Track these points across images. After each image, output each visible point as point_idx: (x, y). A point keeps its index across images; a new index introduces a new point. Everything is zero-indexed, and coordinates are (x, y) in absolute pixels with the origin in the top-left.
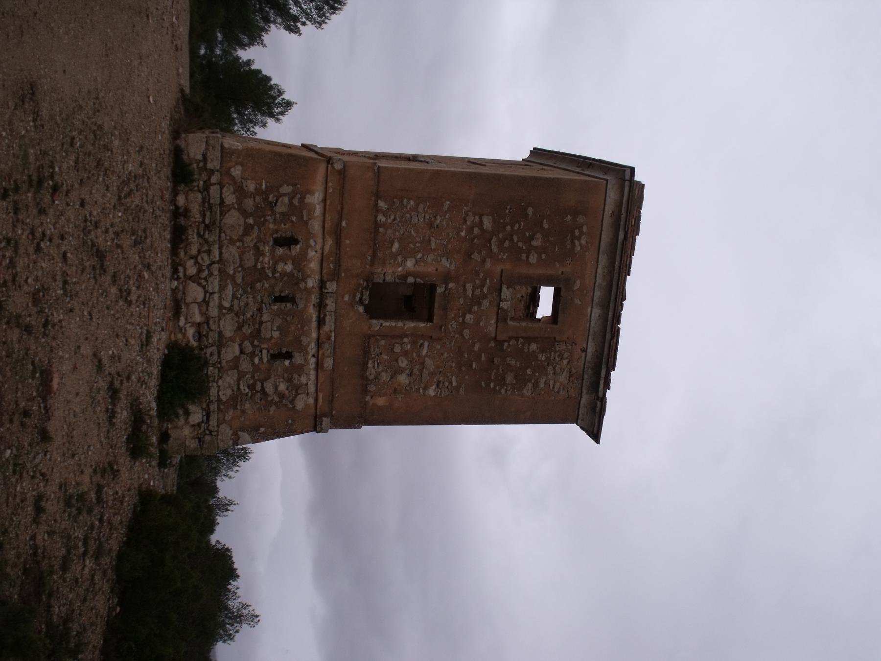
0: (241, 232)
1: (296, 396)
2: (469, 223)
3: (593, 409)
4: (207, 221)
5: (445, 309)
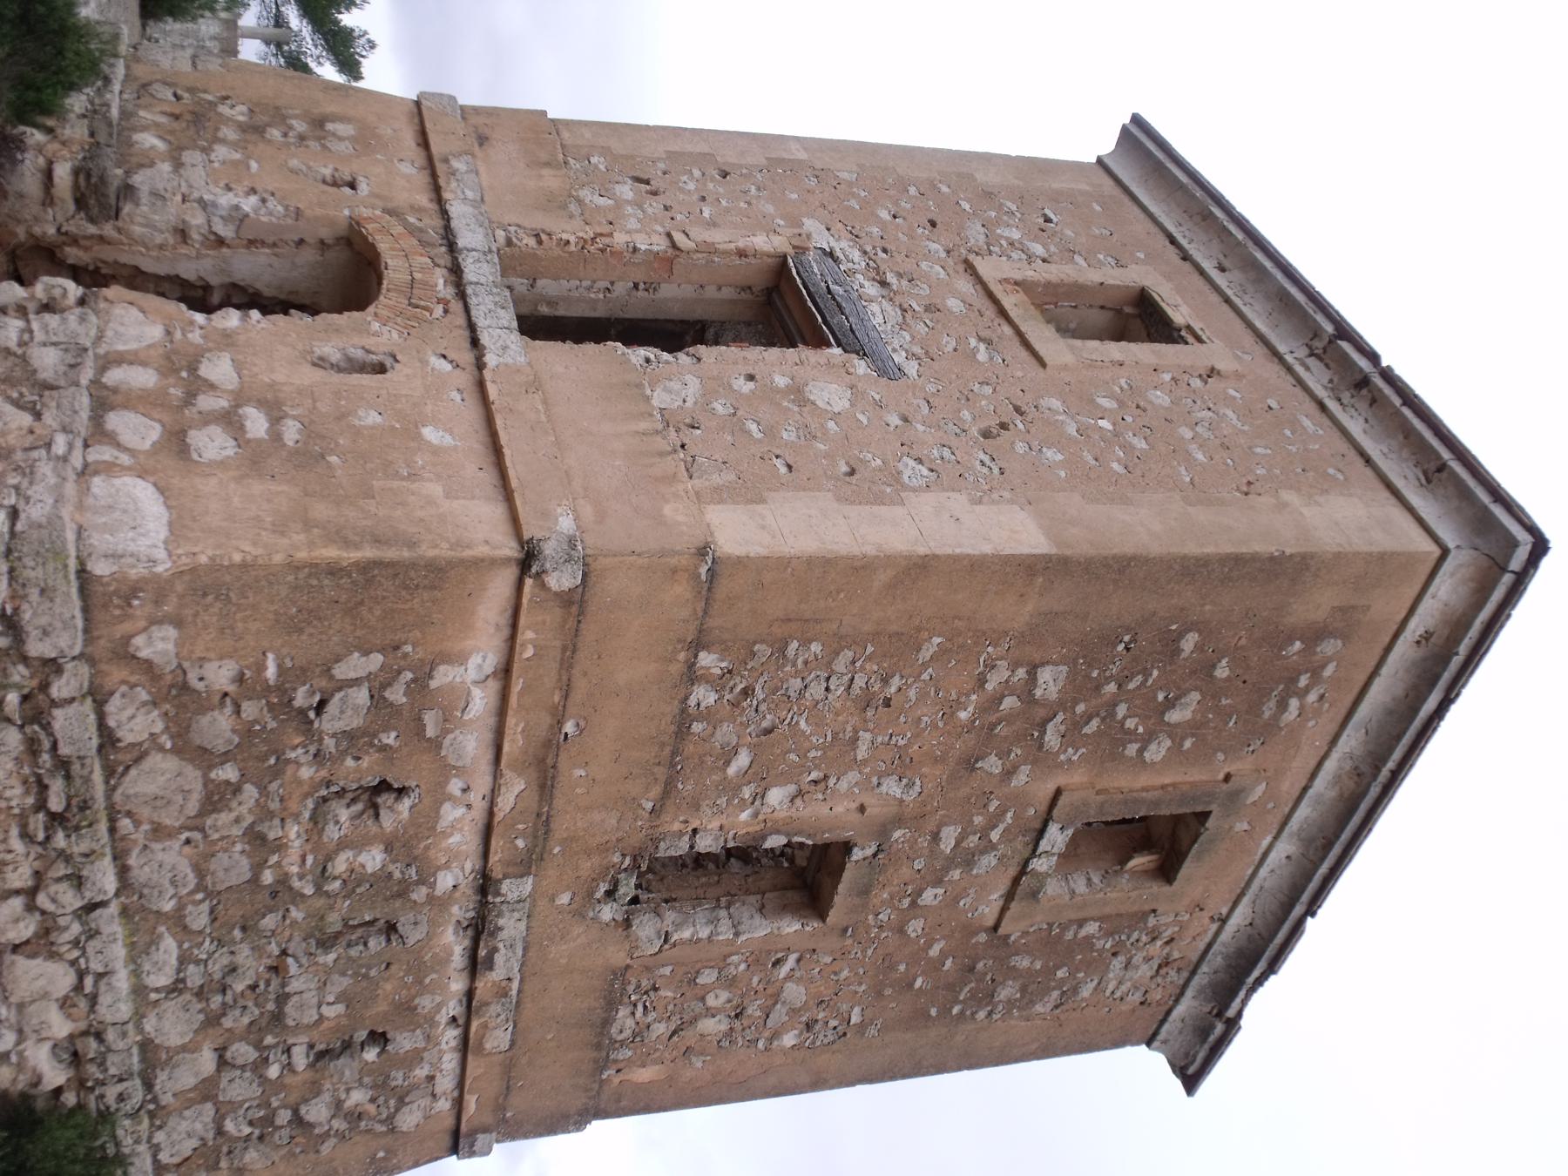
0: (193, 807)
1: (397, 1110)
2: (989, 687)
3: (1203, 1032)
4: (56, 803)
5: (865, 891)
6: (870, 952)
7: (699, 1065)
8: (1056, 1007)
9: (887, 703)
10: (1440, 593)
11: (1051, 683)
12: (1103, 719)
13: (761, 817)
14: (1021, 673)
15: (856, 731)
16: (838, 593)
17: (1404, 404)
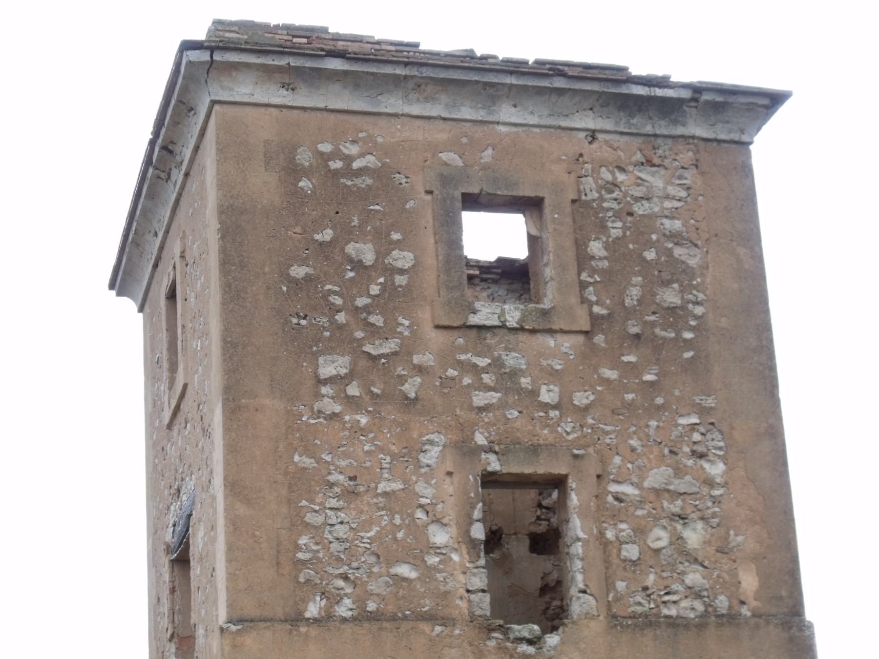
2: (338, 409)
3: (717, 108)
5: (535, 450)
6: (608, 428)
7: (740, 539)
8: (696, 246)
9: (353, 478)
10: (248, 92)
11: (336, 364)
12: (369, 313)
13: (456, 546)
14: (325, 390)
15: (378, 495)
16: (255, 536)
17: (163, 124)
